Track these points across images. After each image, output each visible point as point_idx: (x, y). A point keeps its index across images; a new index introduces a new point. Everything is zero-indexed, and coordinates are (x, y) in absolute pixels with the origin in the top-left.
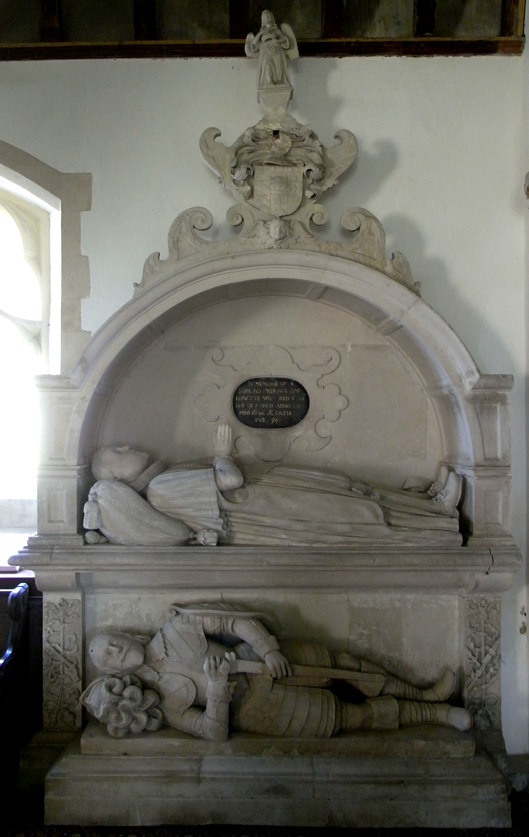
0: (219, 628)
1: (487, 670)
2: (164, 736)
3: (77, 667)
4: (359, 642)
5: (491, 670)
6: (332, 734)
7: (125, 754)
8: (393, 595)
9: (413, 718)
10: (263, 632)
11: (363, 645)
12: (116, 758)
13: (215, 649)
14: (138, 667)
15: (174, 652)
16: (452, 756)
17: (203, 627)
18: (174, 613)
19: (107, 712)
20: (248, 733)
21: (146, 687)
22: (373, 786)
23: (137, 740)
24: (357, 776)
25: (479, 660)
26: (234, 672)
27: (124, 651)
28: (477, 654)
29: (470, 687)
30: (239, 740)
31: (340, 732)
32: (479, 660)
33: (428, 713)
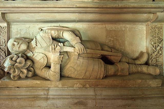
0: (57, 35)
1: (158, 52)
2: (34, 79)
3: (5, 52)
4: (109, 43)
5: (160, 52)
6: (103, 78)
7: (18, 87)
8: (122, 25)
9: (134, 70)
10: (75, 36)
11: (111, 44)
12: (13, 89)
13: (55, 42)
14: (25, 51)
15: (39, 44)
16: (152, 86)
17: (51, 34)
18: (40, 30)
19: (10, 68)
20: (69, 78)
21: (27, 58)
22: (121, 100)
23: (22, 81)
24: (113, 96)
25: (156, 49)
26: (62, 51)
27: (20, 44)
28: (154, 46)
29: (152, 59)
30: (64, 81)
31: (106, 77)
32: (156, 49)
33: (139, 69)
